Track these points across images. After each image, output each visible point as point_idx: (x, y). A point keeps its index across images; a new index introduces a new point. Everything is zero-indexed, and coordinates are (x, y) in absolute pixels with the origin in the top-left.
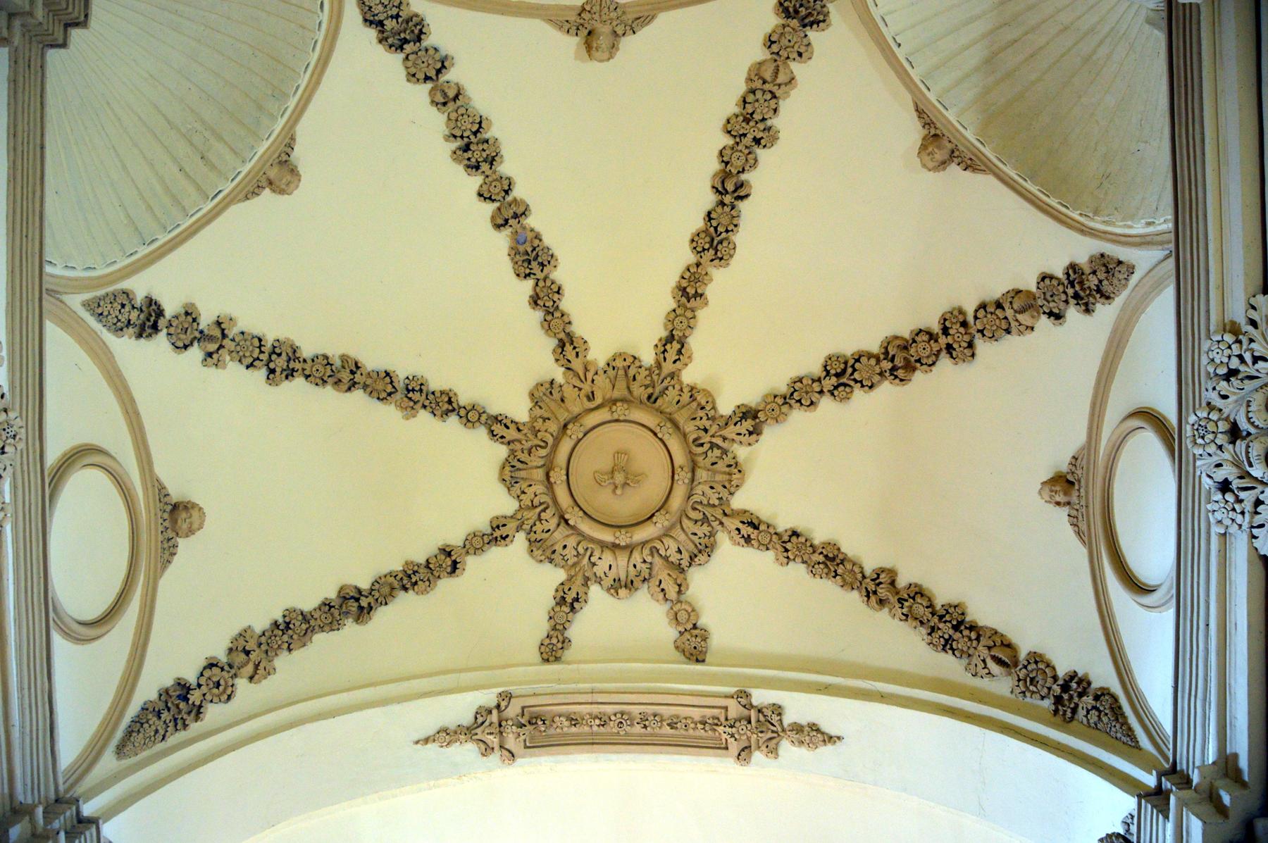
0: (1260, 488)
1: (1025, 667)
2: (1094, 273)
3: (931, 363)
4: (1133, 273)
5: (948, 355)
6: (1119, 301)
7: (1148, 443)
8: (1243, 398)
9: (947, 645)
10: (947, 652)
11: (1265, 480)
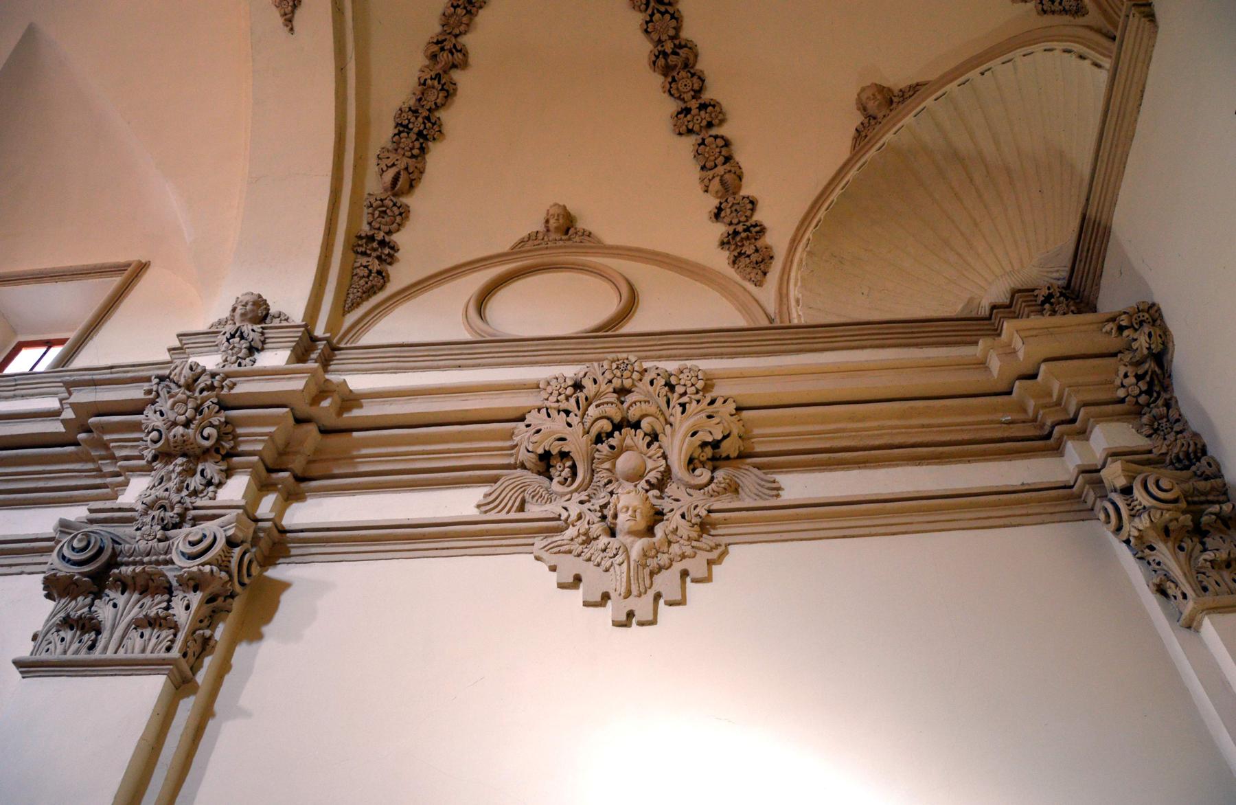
0: (579, 413)
1: (395, 205)
2: (757, 251)
3: (672, 92)
4: (756, 285)
5: (680, 110)
6: (731, 272)
7: (609, 306)
8: (651, 396)
9: (402, 128)
10: (396, 127)
11: (585, 416)
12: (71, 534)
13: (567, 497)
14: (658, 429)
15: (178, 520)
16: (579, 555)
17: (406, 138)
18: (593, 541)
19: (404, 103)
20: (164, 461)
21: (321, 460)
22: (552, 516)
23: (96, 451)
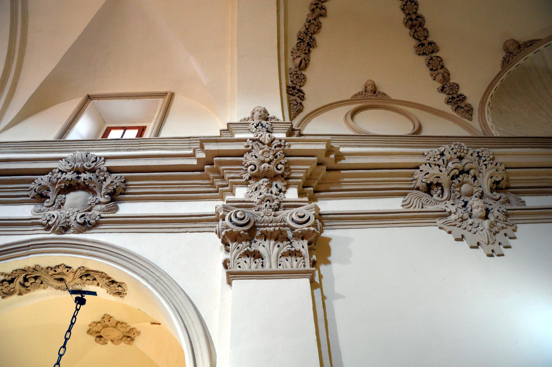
0: (444, 166)
3: (415, 36)
4: (469, 120)
9: (301, 40)
12: (229, 212)
13: (445, 202)
14: (477, 175)
15: (277, 207)
16: (460, 227)
17: (303, 45)
18: (464, 221)
19: (301, 29)
20: (255, 180)
21: (324, 183)
22: (442, 210)
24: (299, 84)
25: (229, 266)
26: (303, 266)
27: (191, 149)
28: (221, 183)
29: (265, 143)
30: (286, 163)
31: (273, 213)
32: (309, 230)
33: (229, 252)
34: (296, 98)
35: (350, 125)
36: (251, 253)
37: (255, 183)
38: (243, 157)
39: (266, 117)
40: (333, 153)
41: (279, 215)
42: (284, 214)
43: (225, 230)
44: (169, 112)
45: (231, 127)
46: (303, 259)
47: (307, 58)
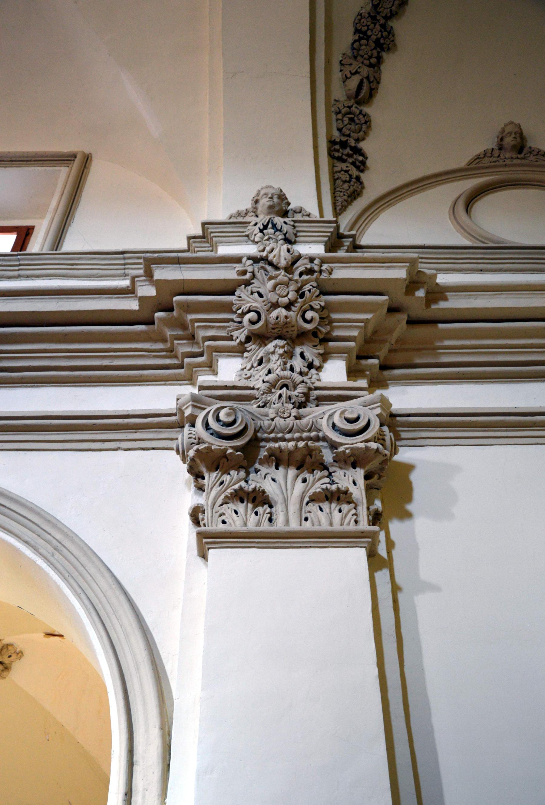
12: (204, 409)
15: (303, 399)
20: (258, 342)
23: (173, 330)
24: (355, 135)
25: (203, 519)
26: (354, 523)
27: (126, 277)
28: (188, 349)
29: (279, 265)
30: (323, 308)
31: (294, 412)
32: (367, 448)
33: (204, 491)
34: (347, 167)
35: (462, 224)
36: (248, 494)
37: (258, 349)
38: (234, 295)
39: (282, 209)
40: (423, 287)
41: (308, 416)
42: (317, 414)
43: (196, 447)
44: (80, 197)
45: (210, 230)
46: (355, 508)
47: (374, 77)
